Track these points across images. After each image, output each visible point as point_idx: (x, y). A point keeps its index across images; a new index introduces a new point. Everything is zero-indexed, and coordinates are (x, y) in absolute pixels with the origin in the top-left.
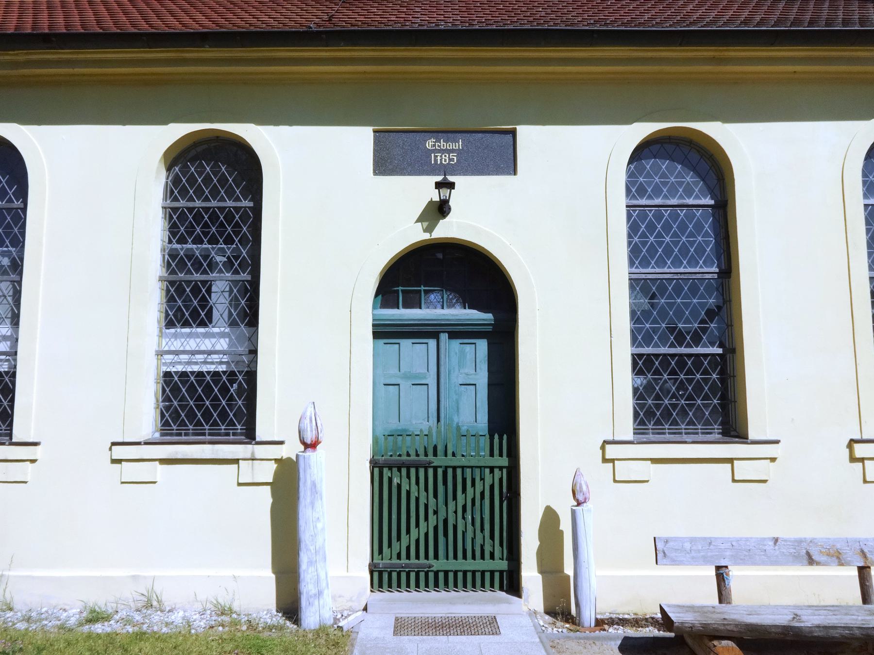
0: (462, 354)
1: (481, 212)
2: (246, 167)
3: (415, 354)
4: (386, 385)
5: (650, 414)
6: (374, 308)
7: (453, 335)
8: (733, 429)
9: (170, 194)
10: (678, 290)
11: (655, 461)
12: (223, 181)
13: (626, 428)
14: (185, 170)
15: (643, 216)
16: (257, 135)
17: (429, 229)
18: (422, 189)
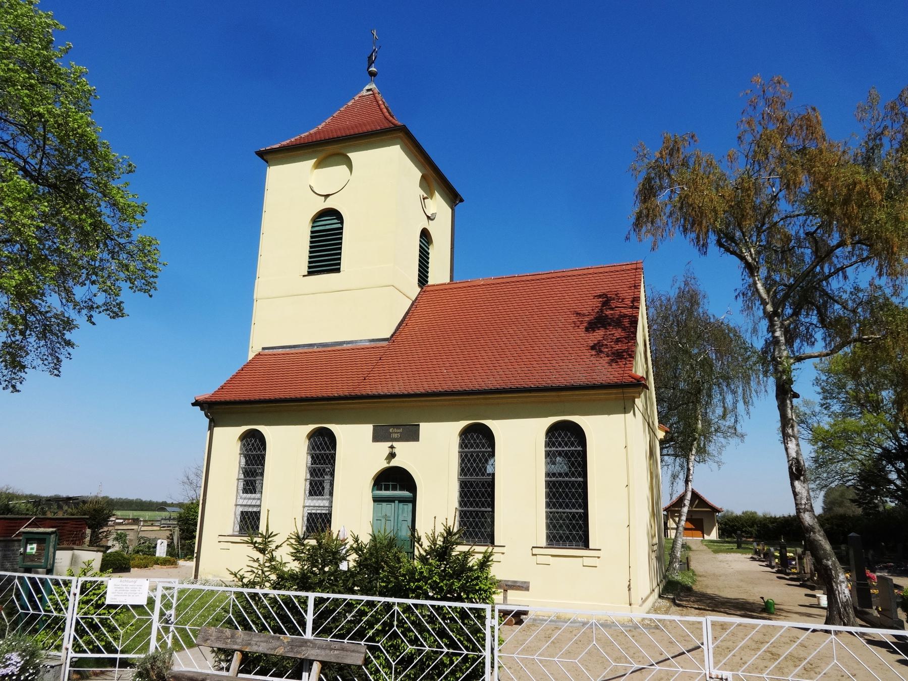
0: (403, 509)
1: (407, 456)
2: (488, 436)
3: (387, 508)
4: (376, 519)
5: (554, 537)
6: (373, 490)
7: (400, 502)
8: (586, 546)
9: (461, 446)
10: (477, 485)
11: (553, 556)
12: (326, 443)
13: (543, 542)
14: (466, 437)
15: (466, 456)
16: (334, 428)
17: (389, 463)
18: (383, 448)
